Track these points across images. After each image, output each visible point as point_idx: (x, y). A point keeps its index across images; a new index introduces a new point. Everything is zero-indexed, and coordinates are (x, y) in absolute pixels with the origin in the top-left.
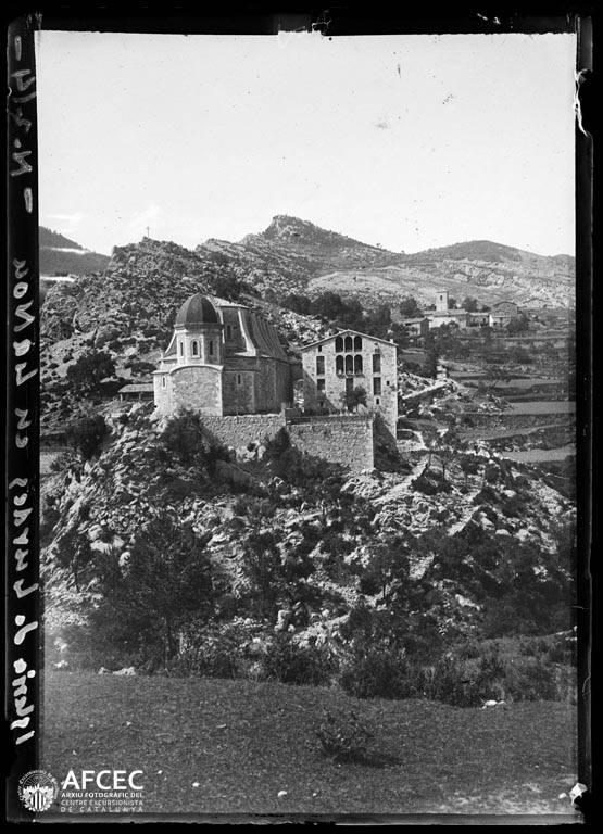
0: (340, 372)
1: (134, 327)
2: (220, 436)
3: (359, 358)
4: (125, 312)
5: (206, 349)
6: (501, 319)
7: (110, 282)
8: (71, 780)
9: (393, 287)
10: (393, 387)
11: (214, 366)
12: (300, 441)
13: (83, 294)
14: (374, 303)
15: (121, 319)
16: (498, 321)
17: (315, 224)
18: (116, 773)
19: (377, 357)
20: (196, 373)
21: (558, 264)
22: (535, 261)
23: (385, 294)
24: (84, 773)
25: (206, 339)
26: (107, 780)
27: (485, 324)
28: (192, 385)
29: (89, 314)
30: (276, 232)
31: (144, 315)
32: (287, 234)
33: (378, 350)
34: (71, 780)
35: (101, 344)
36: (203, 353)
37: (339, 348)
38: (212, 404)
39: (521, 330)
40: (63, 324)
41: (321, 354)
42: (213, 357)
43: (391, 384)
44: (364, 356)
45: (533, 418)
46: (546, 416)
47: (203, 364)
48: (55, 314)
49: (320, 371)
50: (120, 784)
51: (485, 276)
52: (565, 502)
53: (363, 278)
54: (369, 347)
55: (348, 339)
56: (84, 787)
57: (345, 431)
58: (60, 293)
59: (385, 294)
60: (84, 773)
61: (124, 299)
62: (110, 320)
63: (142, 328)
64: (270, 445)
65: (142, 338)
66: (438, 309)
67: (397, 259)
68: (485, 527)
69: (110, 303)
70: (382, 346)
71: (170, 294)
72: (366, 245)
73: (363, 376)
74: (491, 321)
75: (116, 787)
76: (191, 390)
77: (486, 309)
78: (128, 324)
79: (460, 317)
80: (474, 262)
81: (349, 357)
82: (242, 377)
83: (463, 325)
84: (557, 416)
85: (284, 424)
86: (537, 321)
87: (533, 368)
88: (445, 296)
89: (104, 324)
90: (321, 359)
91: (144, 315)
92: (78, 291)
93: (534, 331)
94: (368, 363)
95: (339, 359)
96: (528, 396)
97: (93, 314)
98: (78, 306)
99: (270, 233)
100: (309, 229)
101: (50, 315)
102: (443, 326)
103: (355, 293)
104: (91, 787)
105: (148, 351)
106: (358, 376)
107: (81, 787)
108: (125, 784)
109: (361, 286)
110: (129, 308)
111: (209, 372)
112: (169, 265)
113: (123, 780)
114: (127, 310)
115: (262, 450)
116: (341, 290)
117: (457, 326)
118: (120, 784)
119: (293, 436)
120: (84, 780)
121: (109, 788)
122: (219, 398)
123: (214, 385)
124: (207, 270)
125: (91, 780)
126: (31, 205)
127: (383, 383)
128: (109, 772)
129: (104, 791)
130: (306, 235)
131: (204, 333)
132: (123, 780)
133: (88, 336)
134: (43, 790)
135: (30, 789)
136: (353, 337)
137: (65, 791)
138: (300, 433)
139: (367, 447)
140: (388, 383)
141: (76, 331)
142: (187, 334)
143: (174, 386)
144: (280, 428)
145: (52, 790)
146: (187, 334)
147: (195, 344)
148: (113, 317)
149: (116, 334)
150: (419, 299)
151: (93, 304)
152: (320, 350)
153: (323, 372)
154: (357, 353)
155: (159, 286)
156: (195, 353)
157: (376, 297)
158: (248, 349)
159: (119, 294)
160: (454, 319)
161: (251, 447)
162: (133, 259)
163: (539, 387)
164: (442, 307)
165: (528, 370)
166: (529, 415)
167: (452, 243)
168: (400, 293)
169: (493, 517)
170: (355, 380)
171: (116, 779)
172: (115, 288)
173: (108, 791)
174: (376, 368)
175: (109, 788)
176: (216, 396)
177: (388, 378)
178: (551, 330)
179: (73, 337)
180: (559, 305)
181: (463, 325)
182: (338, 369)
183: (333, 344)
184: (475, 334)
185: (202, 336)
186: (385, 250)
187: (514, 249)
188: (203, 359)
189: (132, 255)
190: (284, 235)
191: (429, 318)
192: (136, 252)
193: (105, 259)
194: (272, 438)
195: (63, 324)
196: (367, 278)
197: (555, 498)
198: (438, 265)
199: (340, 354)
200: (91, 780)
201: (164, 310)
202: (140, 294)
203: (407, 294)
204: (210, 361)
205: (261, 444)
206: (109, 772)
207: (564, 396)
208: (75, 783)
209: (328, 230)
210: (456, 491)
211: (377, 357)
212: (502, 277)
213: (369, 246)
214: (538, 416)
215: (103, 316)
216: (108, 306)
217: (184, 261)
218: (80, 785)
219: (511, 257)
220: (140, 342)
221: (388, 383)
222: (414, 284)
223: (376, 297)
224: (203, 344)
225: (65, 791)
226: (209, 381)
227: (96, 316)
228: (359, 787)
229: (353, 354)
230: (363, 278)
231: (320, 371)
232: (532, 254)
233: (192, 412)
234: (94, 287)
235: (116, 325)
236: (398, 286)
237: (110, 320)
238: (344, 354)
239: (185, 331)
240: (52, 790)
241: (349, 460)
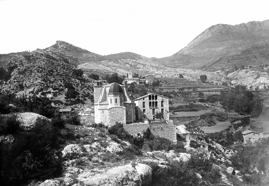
0: (150, 107)
3: (156, 102)
5: (120, 101)
6: (150, 81)
7: (35, 70)
9: (109, 69)
10: (167, 112)
12: (153, 132)
13: (25, 74)
15: (42, 84)
16: (149, 82)
19: (162, 102)
21: (154, 61)
22: (147, 59)
23: (106, 71)
25: (120, 98)
27: (145, 83)
29: (30, 82)
31: (50, 82)
32: (63, 48)
33: (163, 100)
35: (37, 93)
36: (119, 103)
37: (150, 99)
38: (122, 120)
39: (157, 85)
40: (20, 85)
41: (144, 101)
42: (122, 104)
43: (167, 111)
44: (158, 102)
45: (186, 118)
48: (16, 81)
49: (144, 106)
51: (136, 65)
52: (225, 148)
54: (159, 99)
57: (167, 128)
59: (106, 71)
61: (42, 76)
62: (38, 84)
63: (52, 87)
64: (145, 134)
65: (52, 91)
66: (129, 77)
68: (214, 158)
73: (158, 108)
74: (147, 82)
76: (115, 115)
77: (144, 78)
78: (46, 85)
79: (137, 80)
80: (132, 60)
81: (153, 102)
82: (130, 110)
84: (193, 117)
85: (149, 126)
87: (175, 100)
88: (131, 73)
89: (37, 86)
90: (144, 103)
91: (50, 82)
92: (24, 73)
93: (161, 86)
94: (159, 104)
95: (150, 103)
97: (31, 82)
98: (25, 79)
99: (55, 46)
100: (71, 46)
101: (15, 82)
102: (132, 83)
103: (95, 70)
105: (57, 96)
106: (156, 108)
111: (121, 109)
115: (142, 135)
117: (136, 83)
119: (152, 131)
122: (125, 118)
123: (123, 113)
124: (62, 65)
126: (215, 88)
136: (155, 95)
138: (154, 129)
139: (175, 133)
140: (166, 110)
142: (113, 96)
143: (110, 114)
144: (147, 128)
146: (113, 96)
147: (116, 100)
148: (39, 83)
150: (118, 73)
151: (31, 78)
152: (144, 100)
153: (145, 107)
154: (156, 101)
155: (52, 71)
156: (116, 103)
157: (103, 72)
159: (40, 74)
160: (135, 81)
161: (139, 135)
164: (130, 77)
165: (173, 100)
166: (185, 117)
168: (111, 70)
170: (155, 109)
172: (37, 72)
174: (162, 106)
176: (124, 117)
177: (166, 109)
178: (166, 85)
180: (165, 76)
182: (150, 106)
183: (148, 98)
184: (143, 86)
187: (140, 55)
190: (62, 48)
194: (145, 131)
195: (20, 85)
196: (99, 65)
197: (221, 147)
198: (119, 61)
199: (151, 101)
203: (113, 71)
204: (121, 105)
205: (142, 133)
211: (162, 102)
212: (142, 66)
214: (188, 117)
215: (36, 82)
216: (36, 79)
217: (53, 61)
220: (52, 92)
221: (166, 110)
222: (115, 68)
223: (103, 72)
224: (119, 100)
226: (122, 112)
227: (33, 82)
229: (155, 101)
231: (144, 106)
232: (146, 57)
233: (120, 123)
235: (41, 86)
236: (109, 68)
237: (38, 84)
238: (152, 101)
239: (113, 95)
241: (169, 138)
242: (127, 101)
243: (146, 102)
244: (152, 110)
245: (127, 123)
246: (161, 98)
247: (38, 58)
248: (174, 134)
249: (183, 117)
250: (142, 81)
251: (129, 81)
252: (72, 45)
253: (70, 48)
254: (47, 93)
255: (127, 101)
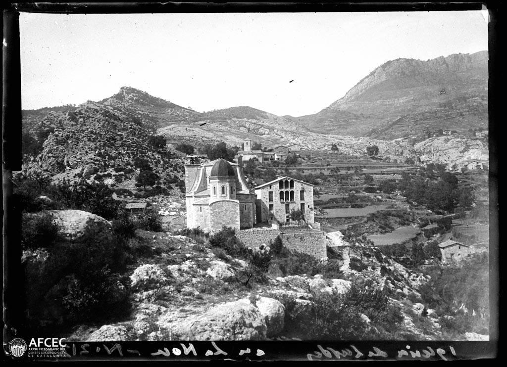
1: (106, 166)
2: (244, 242)
3: (292, 193)
4: (99, 156)
5: (230, 191)
6: (282, 156)
8: (33, 342)
9: (210, 135)
10: (311, 209)
11: (234, 200)
12: (287, 243)
13: (68, 144)
14: (200, 144)
15: (97, 160)
16: (280, 157)
17: (149, 94)
18: (53, 339)
19: (302, 192)
20: (225, 205)
21: (289, 121)
22: (276, 119)
23: (206, 139)
24: (39, 339)
25: (230, 185)
26: (49, 342)
27: (272, 159)
28: (222, 211)
29: (76, 157)
30: (124, 97)
31: (111, 158)
32: (132, 99)
33: (303, 188)
34: (33, 342)
35: (88, 176)
36: (228, 194)
37: (281, 187)
38: (234, 222)
40: (58, 163)
42: (232, 195)
43: (310, 207)
44: (295, 191)
45: (344, 219)
46: (350, 218)
47: (228, 200)
48: (52, 156)
49: (271, 200)
50: (55, 344)
52: (409, 271)
53: (190, 129)
54: (297, 187)
55: (287, 182)
56: (39, 346)
58: (54, 144)
59: (206, 139)
60: (39, 339)
61: (96, 148)
62: (90, 161)
63: (113, 166)
64: (272, 246)
65: (114, 173)
66: (245, 150)
67: (201, 116)
68: (391, 289)
69: (88, 150)
70: (305, 186)
71: (122, 145)
72: (181, 107)
73: (295, 202)
74: (276, 157)
75: (53, 346)
76: (222, 214)
77: (271, 151)
78: (102, 163)
79: (259, 155)
80: (250, 120)
81: (287, 192)
82: (247, 207)
83: (261, 160)
84: (356, 218)
85: (279, 234)
86: (300, 157)
88: (249, 142)
89: (87, 164)
90: (271, 193)
91: (111, 158)
94: (297, 195)
95: (281, 193)
96: (329, 205)
97: (78, 157)
98: (66, 152)
99: (119, 97)
100: (146, 95)
101: (49, 157)
102: (250, 160)
104: (42, 345)
105: (121, 182)
106: (292, 203)
107: (37, 345)
108: (58, 344)
109: (191, 134)
110: (101, 153)
112: (108, 125)
113: (57, 342)
114: (99, 155)
115: (268, 249)
116: (179, 136)
118: (55, 344)
119: (284, 241)
120: (39, 342)
121: (50, 346)
122: (238, 219)
123: (235, 211)
124: (131, 128)
125: (42, 342)
127: (306, 206)
128: (50, 339)
129: (48, 348)
130: (144, 100)
131: (229, 182)
132: (57, 342)
133: (77, 171)
134: (20, 347)
135: (14, 347)
136: (289, 181)
137: (30, 348)
139: (323, 246)
140: (309, 206)
141: (68, 168)
142: (219, 182)
143: (212, 212)
144: (276, 236)
145: (24, 347)
146: (219, 182)
147: (223, 188)
148: (91, 159)
149: (96, 171)
150: (226, 143)
152: (271, 188)
153: (272, 201)
154: (292, 190)
156: (223, 193)
157: (201, 141)
158: (243, 189)
160: (255, 156)
161: (262, 248)
162: (81, 120)
163: (333, 200)
164: (247, 149)
165: (321, 189)
166: (341, 218)
167: (228, 107)
169: (393, 283)
170: (290, 205)
171: (53, 342)
172: (88, 141)
173: (50, 348)
174: (302, 198)
175: (50, 346)
176: (236, 218)
177: (309, 204)
178: (309, 163)
179: (67, 172)
181: (261, 160)
182: (281, 199)
183: (278, 185)
184: (269, 165)
185: (227, 184)
186: (194, 111)
187: (264, 112)
188: (228, 197)
189: (81, 117)
190: (130, 99)
191: (242, 155)
192: (83, 115)
193: (325, 154)
194: (273, 241)
195: (58, 163)
197: (404, 269)
199: (282, 190)
200: (42, 342)
201: (122, 155)
202: (105, 145)
203: (219, 139)
204: (231, 197)
206: (50, 339)
207: (348, 205)
208: (35, 344)
209: (157, 97)
210: (370, 269)
211: (302, 192)
212: (268, 130)
213: (184, 108)
214: (346, 218)
215: (85, 158)
216: (87, 152)
217: (116, 122)
218: (37, 345)
219: (262, 117)
221: (309, 206)
222: (221, 133)
223: (201, 141)
224: (228, 188)
225: (30, 348)
226: (232, 209)
227: (81, 158)
228: (88, 318)
230: (190, 129)
231: (271, 200)
233: (231, 228)
234: (74, 140)
235: (95, 164)
237: (90, 161)
238: (284, 190)
239: (218, 180)
240: (24, 347)
242: (242, 190)
243: (274, 193)
244: (284, 205)
245: (242, 228)
246: (299, 184)
247: (89, 117)
248: (322, 247)
249: (338, 218)
250: (267, 157)
251: (246, 156)
252: (147, 93)
253: (144, 99)
254: (105, 176)
255: (242, 190)
